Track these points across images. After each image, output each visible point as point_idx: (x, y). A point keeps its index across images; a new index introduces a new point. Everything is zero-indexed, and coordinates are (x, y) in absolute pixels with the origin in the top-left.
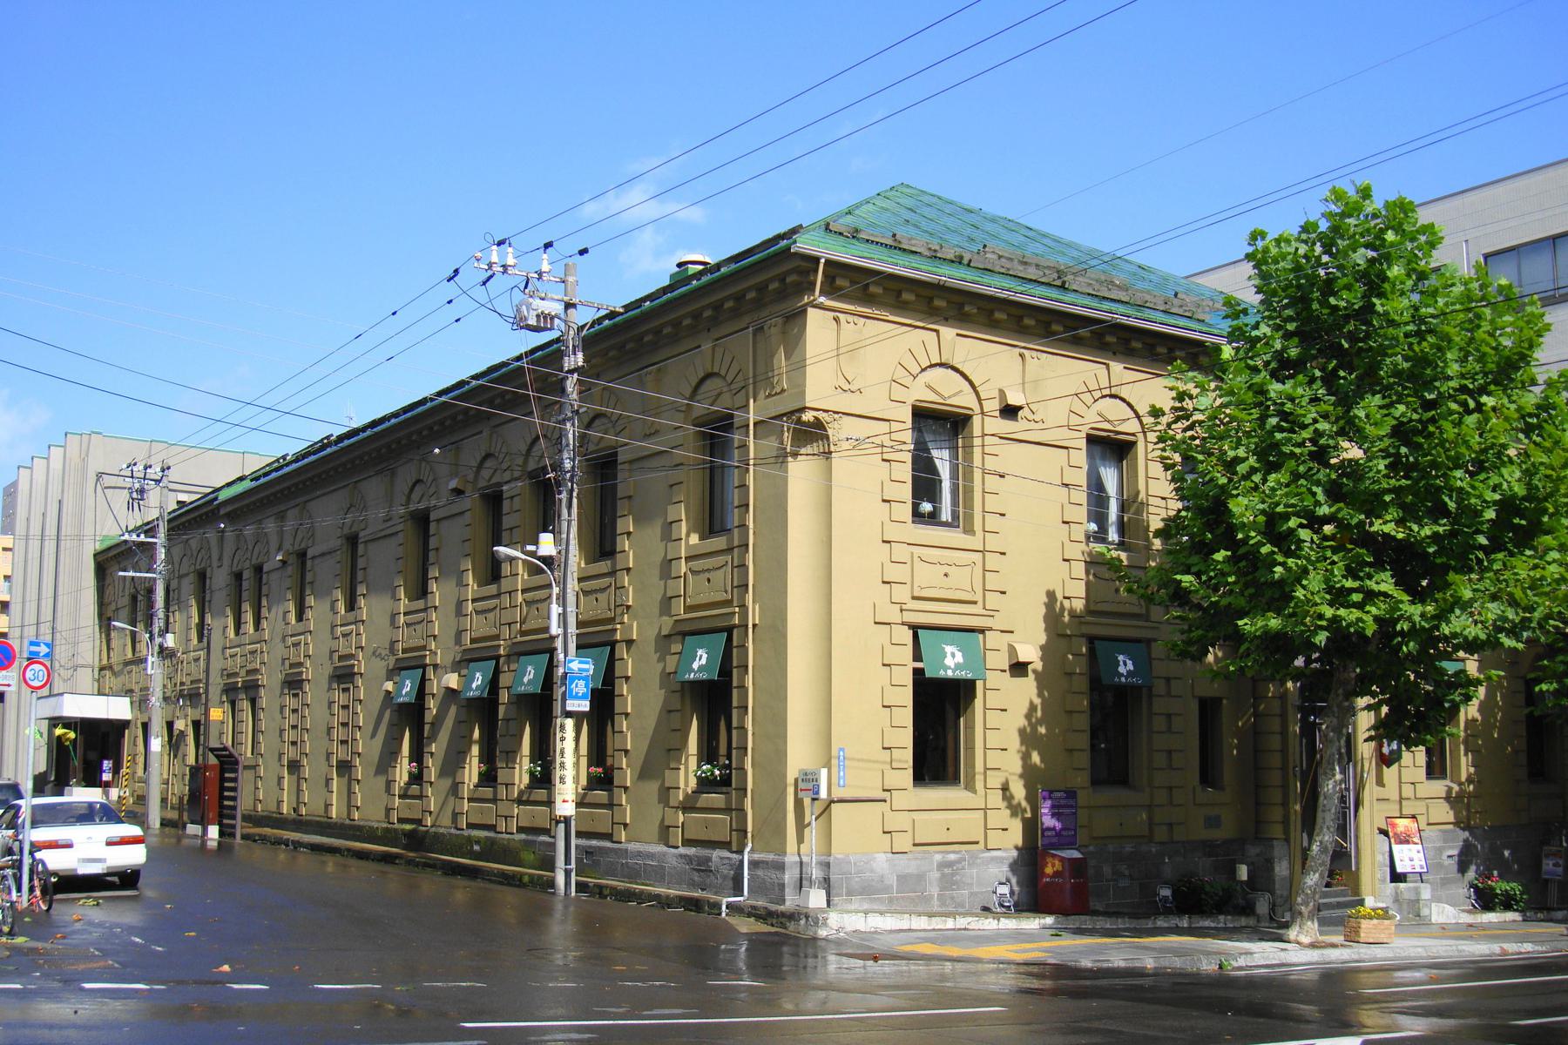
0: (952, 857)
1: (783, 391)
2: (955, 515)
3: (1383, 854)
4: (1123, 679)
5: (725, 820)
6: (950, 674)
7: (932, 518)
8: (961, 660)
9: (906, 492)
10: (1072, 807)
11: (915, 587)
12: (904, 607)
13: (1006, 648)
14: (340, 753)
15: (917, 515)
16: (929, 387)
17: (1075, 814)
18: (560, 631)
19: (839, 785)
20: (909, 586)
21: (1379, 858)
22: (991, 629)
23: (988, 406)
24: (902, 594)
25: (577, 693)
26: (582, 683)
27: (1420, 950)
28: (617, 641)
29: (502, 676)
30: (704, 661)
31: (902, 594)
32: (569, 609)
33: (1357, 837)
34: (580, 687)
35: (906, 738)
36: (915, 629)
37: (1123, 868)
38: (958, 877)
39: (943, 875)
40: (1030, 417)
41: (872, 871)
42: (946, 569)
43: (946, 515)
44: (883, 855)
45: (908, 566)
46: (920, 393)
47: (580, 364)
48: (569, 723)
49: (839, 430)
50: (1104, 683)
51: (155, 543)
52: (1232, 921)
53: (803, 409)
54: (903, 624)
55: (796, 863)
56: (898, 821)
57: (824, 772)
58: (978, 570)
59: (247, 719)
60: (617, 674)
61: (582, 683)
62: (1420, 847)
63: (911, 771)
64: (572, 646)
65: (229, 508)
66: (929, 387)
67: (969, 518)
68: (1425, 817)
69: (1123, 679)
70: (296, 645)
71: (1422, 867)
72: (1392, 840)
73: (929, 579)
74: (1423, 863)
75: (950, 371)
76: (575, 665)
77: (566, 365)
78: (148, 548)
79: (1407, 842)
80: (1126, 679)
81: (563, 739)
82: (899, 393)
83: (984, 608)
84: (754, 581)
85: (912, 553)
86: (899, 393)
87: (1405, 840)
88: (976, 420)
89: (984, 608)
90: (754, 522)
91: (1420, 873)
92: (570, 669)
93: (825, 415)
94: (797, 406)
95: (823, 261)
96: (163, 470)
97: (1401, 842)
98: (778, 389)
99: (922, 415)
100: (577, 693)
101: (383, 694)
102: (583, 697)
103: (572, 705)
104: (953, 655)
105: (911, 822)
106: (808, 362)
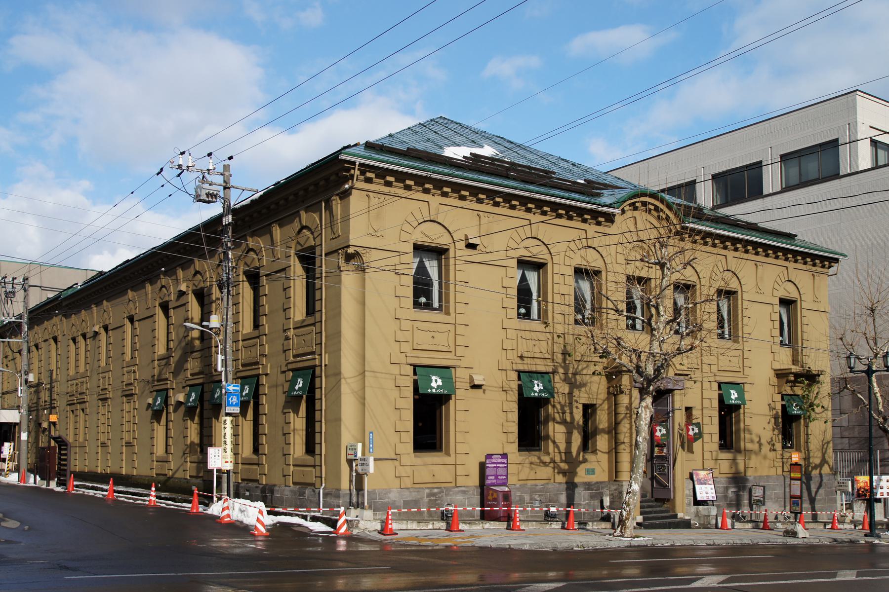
0: (436, 491)
1: (339, 236)
2: (440, 306)
3: (689, 490)
4: (733, 402)
5: (311, 471)
6: (434, 391)
7: (428, 306)
8: (441, 384)
9: (410, 292)
10: (504, 463)
11: (415, 343)
12: (408, 355)
13: (468, 377)
14: (126, 437)
15: (417, 305)
16: (423, 233)
17: (507, 467)
18: (223, 369)
19: (370, 452)
20: (411, 343)
21: (687, 492)
22: (459, 367)
23: (703, 282)
24: (406, 348)
25: (232, 403)
26: (235, 397)
27: (690, 541)
28: (259, 375)
29: (205, 394)
30: (301, 385)
31: (406, 348)
32: (228, 357)
33: (674, 480)
34: (234, 400)
35: (514, 428)
36: (415, 366)
37: (537, 497)
38: (439, 501)
39: (430, 500)
40: (484, 250)
41: (389, 498)
42: (433, 334)
43: (436, 304)
44: (395, 490)
45: (410, 333)
46: (418, 237)
47: (230, 221)
48: (229, 419)
49: (369, 257)
50: (726, 403)
51: (21, 322)
52: (597, 526)
53: (348, 246)
54: (407, 364)
55: (346, 494)
56: (402, 471)
57: (360, 446)
58: (452, 334)
59: (80, 415)
60: (261, 392)
61: (235, 397)
62: (713, 486)
63: (517, 444)
64: (230, 377)
65: (67, 302)
66: (423, 233)
67: (448, 308)
68: (718, 470)
69: (733, 402)
70: (104, 378)
71: (713, 497)
72: (696, 483)
73: (422, 339)
74: (714, 495)
75: (436, 224)
76: (231, 388)
77: (224, 222)
78: (19, 325)
79: (705, 484)
80: (436, 390)
81: (225, 428)
82: (404, 236)
83: (455, 355)
84: (326, 340)
85: (413, 326)
86: (404, 236)
87: (702, 483)
88: (549, 266)
89: (455, 355)
90: (325, 308)
91: (713, 500)
92: (228, 389)
93: (361, 249)
94: (346, 244)
95: (357, 163)
96: (24, 280)
97: (701, 484)
98: (337, 235)
99: (419, 249)
100: (232, 403)
101: (146, 405)
102: (236, 405)
103: (229, 410)
104: (436, 381)
105: (412, 472)
106: (351, 216)
